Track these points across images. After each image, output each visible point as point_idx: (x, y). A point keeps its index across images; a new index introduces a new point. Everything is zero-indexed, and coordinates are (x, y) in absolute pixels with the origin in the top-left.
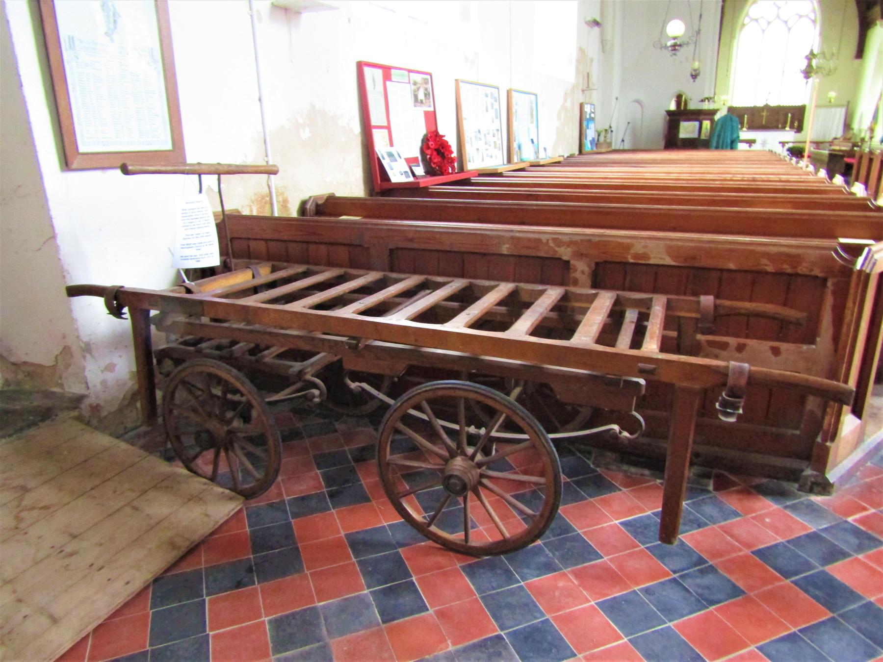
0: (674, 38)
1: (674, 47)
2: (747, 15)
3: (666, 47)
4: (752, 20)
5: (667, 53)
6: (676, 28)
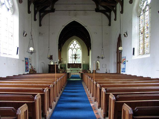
0: (31, 51)
1: (31, 52)
2: (69, 47)
3: (29, 53)
4: (70, 48)
5: (30, 54)
6: (31, 49)
